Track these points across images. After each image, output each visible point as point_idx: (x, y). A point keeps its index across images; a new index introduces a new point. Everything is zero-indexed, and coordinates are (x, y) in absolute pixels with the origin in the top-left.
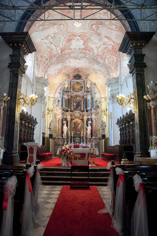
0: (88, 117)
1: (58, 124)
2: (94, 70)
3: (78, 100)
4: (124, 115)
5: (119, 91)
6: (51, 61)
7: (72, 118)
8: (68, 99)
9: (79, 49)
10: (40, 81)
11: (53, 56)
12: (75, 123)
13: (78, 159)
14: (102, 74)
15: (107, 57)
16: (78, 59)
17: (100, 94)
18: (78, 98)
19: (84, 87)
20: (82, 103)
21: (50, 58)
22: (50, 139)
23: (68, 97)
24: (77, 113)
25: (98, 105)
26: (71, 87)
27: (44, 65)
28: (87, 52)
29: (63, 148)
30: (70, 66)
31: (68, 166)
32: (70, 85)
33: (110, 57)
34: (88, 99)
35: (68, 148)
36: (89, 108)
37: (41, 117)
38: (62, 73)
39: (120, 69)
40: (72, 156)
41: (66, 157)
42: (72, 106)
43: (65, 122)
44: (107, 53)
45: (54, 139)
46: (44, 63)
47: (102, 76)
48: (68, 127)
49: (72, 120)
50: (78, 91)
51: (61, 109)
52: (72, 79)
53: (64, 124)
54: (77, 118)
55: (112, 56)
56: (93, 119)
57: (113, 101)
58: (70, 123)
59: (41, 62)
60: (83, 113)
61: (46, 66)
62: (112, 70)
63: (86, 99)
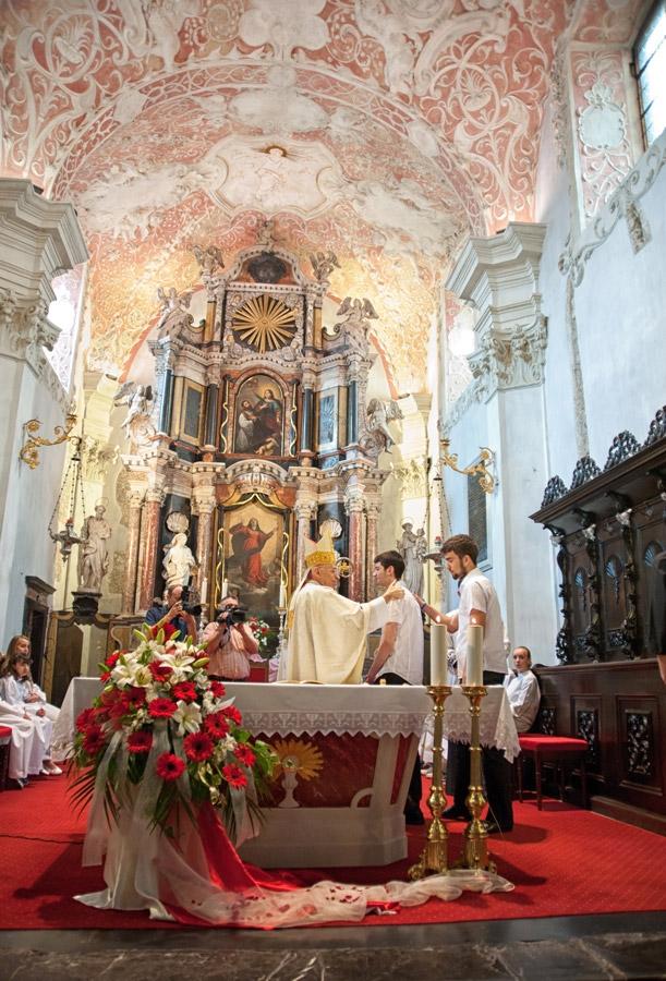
0: (324, 498)
1: (133, 534)
2: (366, 230)
3: (262, 401)
4: (586, 462)
5: (545, 312)
6: (106, 104)
7: (223, 499)
8: (209, 388)
9: (294, 51)
10: (20, 214)
11: (125, 76)
12: (241, 534)
13: (290, 801)
14: (411, 259)
15: (467, 108)
16: (276, 153)
17: (387, 372)
18: (264, 389)
19: (304, 328)
20: (289, 414)
21: (100, 77)
22: (81, 627)
23: (206, 375)
24: (257, 469)
25: (384, 426)
26: (224, 321)
27: (53, 123)
28: (344, 76)
29: (118, 669)
30: (229, 197)
31: (170, 904)
32: (219, 310)
33: (490, 106)
34: (322, 396)
35: (180, 670)
36: (327, 447)
37: (8, 454)
38: (177, 241)
39: (565, 162)
40: (228, 774)
41: (147, 793)
42: (230, 429)
43: (177, 522)
44: (470, 79)
45: (106, 626)
46: (62, 106)
47: (407, 272)
48: (194, 553)
49: (222, 510)
50: (267, 349)
51: (161, 438)
52: (237, 280)
53: (173, 533)
54: (255, 500)
55: (501, 103)
56: (354, 509)
57: (502, 376)
58: (212, 529)
59: (35, 92)
60: (294, 470)
61: (69, 132)
62: (495, 193)
63: (310, 391)
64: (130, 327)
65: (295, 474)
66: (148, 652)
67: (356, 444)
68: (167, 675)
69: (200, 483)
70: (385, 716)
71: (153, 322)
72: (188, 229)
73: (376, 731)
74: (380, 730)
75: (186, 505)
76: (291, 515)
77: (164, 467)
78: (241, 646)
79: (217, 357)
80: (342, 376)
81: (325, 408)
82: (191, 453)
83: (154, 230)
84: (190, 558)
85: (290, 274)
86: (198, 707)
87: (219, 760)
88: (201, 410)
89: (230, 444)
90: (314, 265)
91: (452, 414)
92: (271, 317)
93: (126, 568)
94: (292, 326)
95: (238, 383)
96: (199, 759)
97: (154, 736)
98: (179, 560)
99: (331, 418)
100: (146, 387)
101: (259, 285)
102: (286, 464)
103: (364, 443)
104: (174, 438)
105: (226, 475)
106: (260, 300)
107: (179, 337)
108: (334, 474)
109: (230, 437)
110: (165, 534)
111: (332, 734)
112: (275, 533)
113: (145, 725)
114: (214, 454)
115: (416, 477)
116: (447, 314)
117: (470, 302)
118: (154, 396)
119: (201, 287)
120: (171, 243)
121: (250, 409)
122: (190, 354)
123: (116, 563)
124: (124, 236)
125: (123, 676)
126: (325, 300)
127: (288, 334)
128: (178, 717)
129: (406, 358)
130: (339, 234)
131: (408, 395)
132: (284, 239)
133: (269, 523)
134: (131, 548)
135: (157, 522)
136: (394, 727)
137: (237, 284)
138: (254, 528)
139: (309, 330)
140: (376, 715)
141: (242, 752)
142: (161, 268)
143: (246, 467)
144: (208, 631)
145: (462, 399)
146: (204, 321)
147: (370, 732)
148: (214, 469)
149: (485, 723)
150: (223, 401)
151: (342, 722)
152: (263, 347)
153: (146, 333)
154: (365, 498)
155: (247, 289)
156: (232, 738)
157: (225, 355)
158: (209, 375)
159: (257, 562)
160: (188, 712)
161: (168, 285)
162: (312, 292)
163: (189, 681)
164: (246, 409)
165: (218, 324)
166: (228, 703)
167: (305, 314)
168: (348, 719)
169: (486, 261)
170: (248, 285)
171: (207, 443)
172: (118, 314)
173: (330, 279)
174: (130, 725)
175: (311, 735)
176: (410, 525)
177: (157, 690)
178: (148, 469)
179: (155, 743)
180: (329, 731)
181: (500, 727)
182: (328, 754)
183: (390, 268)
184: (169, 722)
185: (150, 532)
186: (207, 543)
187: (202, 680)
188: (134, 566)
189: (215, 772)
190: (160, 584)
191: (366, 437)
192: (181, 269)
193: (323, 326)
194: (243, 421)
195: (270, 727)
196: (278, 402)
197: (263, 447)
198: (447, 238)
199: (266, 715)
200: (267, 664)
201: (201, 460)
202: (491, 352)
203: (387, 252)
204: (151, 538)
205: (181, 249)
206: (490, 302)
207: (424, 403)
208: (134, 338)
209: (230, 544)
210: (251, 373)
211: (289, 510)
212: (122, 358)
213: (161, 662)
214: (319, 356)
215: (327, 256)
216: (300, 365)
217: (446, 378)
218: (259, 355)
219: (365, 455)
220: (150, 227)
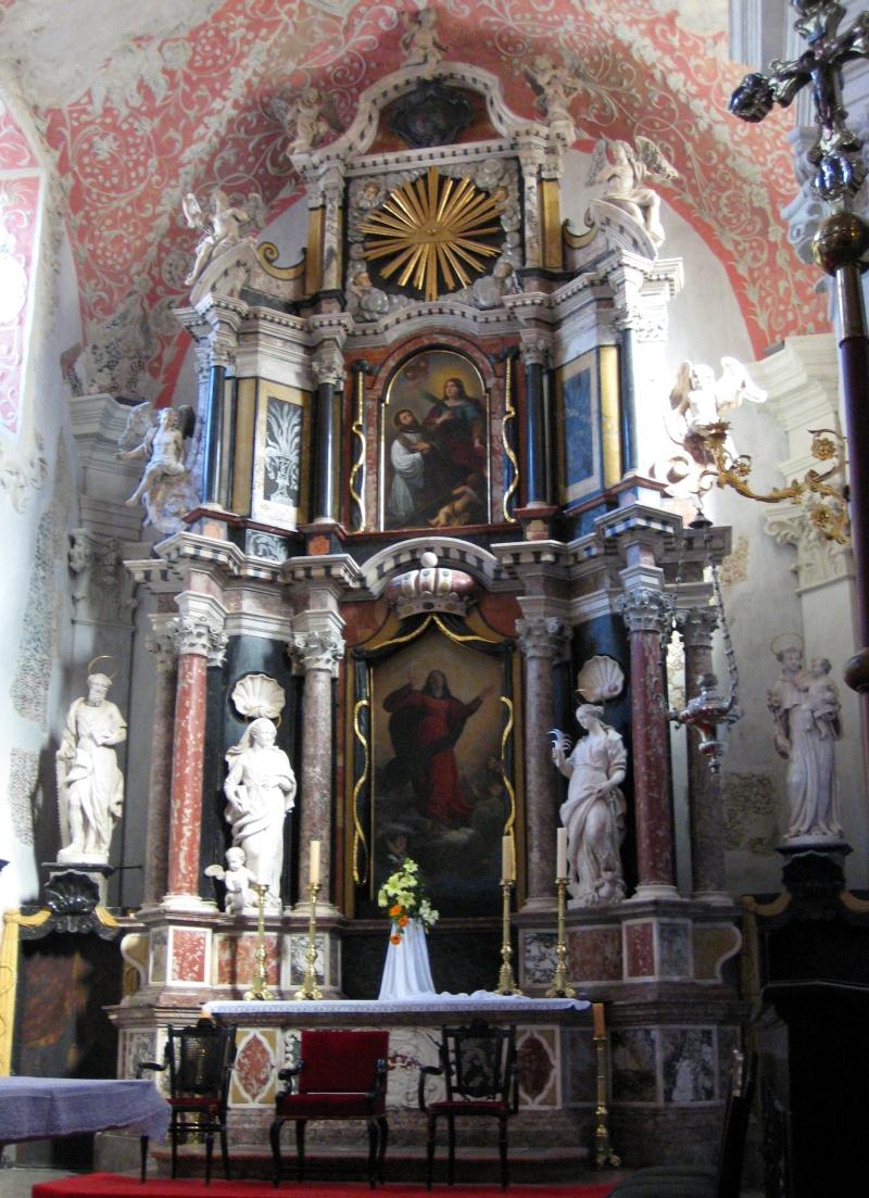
3: (440, 406)
19: (521, 231)
20: (499, 427)
26: (346, 245)
34: (568, 374)
48: (297, 764)
50: (442, 289)
83: (179, 75)
106: (420, 185)
108: (594, 551)
120: (225, 99)
127: (486, 250)
137: (369, 160)
138: (439, 693)
155: (393, 167)
167: (521, 200)
193: (562, 220)
210: (411, 347)
220: (169, 73)
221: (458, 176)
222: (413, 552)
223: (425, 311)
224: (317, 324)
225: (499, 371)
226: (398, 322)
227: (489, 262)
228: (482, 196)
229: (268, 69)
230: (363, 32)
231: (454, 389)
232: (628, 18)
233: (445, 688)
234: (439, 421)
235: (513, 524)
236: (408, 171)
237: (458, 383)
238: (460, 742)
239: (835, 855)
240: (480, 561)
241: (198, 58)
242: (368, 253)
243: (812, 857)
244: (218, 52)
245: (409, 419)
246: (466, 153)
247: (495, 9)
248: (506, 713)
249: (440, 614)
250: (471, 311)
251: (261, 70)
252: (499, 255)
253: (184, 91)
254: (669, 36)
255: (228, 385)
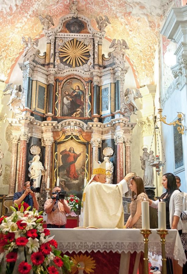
3: (74, 91)
7: (57, 138)
8: (49, 86)
12: (66, 155)
14: (145, 18)
18: (75, 85)
19: (94, 55)
20: (87, 97)
24: (72, 124)
25: (133, 102)
26: (55, 53)
32: (52, 47)
34: (103, 88)
36: (106, 112)
38: (30, 12)
42: (59, 105)
43: (35, 150)
47: (143, 25)
48: (43, 165)
49: (56, 144)
50: (76, 66)
51: (26, 110)
52: (61, 32)
53: (33, 155)
56: (119, 142)
58: (52, 153)
60: (90, 124)
63: (97, 86)
64: (10, 56)
65: (91, 126)
66: (16, 216)
67: (120, 111)
68: (24, 227)
69: (46, 131)
70: (122, 243)
71: (21, 54)
72: (36, 6)
73: (118, 250)
74: (120, 250)
75: (39, 142)
76: (89, 145)
77: (28, 124)
78: (63, 210)
79: (52, 70)
80: (112, 78)
81: (104, 94)
82: (41, 117)
83: (19, 7)
84: (41, 167)
85: (86, 28)
86: (38, 240)
87: (47, 264)
88: (45, 96)
89: (60, 112)
90: (98, 23)
91: (166, 94)
92: (77, 50)
93: (11, 172)
94: (88, 54)
95: (63, 83)
96: (38, 264)
97: (18, 254)
98: (36, 167)
99: (107, 98)
100: (18, 86)
101: (71, 34)
102: (86, 121)
103: (123, 110)
104: (33, 110)
105: (58, 127)
106: (72, 41)
107: (33, 61)
108: (109, 126)
109: (59, 108)
110: (30, 155)
111: (99, 251)
112: (82, 154)
113: (14, 249)
114: (52, 117)
115: (149, 125)
116: (163, 45)
117: (173, 40)
118: (23, 90)
119: (42, 36)
120: (28, 14)
121: (68, 95)
122: (39, 69)
123: (6, 170)
124: (4, 10)
125: (5, 228)
126: (104, 41)
127: (86, 58)
128: (28, 245)
129: (144, 68)
130: (110, 6)
131: (145, 86)
132: (83, 10)
133: (79, 149)
134: (13, 163)
135: (25, 150)
136: (126, 248)
137: (61, 34)
138: (72, 152)
139: (96, 56)
140: (118, 243)
141: (57, 260)
142: (23, 26)
143: (67, 123)
144: (48, 203)
145: (170, 87)
146: (45, 53)
147: (116, 251)
148: (52, 124)
149: (169, 247)
150: (56, 92)
151: (103, 246)
152: (74, 65)
153: (18, 58)
154: (124, 136)
155: (66, 36)
156: (53, 254)
157: (56, 69)
158: (49, 79)
159: (73, 167)
160: (33, 243)
161: (27, 35)
162: (97, 37)
163: (34, 228)
164: (67, 95)
165: (52, 54)
166: (51, 238)
167: (94, 48)
168: (106, 245)
169: (180, 19)
170: (66, 34)
171: (48, 112)
172: (3, 49)
173: (106, 30)
174: (7, 250)
175: (89, 252)
176: (146, 148)
177: (20, 233)
178: (20, 125)
179: (18, 257)
180: (98, 250)
181: (176, 249)
182: (98, 261)
183: (135, 23)
184: (25, 248)
185: (22, 155)
186: (50, 160)
187: (40, 228)
188: (15, 171)
189: (45, 270)
190: (28, 177)
191: (124, 107)
192: (33, 27)
193: (102, 54)
194: (65, 101)
195: (71, 248)
196: (82, 91)
197: (75, 113)
198: (163, 6)
199: (69, 243)
200: (78, 217)
201: (46, 120)
202: (183, 65)
203: (133, 15)
204: (23, 158)
205: (32, 17)
206: (182, 40)
207: (152, 90)
208: (12, 61)
209: (61, 160)
210: (69, 78)
211: (88, 143)
212: (6, 71)
213: (22, 221)
214: (101, 68)
215: (104, 18)
216: (92, 74)
217: (163, 77)
218: (72, 69)
219: (124, 116)
220: (16, 5)
221: (80, 41)
222: (69, 122)
223: (73, 70)
224: (50, 70)
225: (88, 85)
226: (67, 72)
227: (87, 61)
228: (86, 46)
229: (38, 8)
230: (61, 3)
231: (78, 88)
232: (120, 11)
233: (73, 151)
234: (74, 94)
235: (90, 118)
236: (69, 38)
237: (78, 87)
238: (76, 162)
239: (153, 190)
240: (83, 125)
241: (24, 3)
242: (60, 55)
243: (149, 190)
244: (29, 3)
245: (68, 93)
246: (85, 36)
247: (91, 4)
248: (87, 157)
249: (73, 135)
250: (82, 72)
251: (37, 8)
252: (89, 60)
253: (19, 10)
254: (128, 17)
255: (31, 81)
